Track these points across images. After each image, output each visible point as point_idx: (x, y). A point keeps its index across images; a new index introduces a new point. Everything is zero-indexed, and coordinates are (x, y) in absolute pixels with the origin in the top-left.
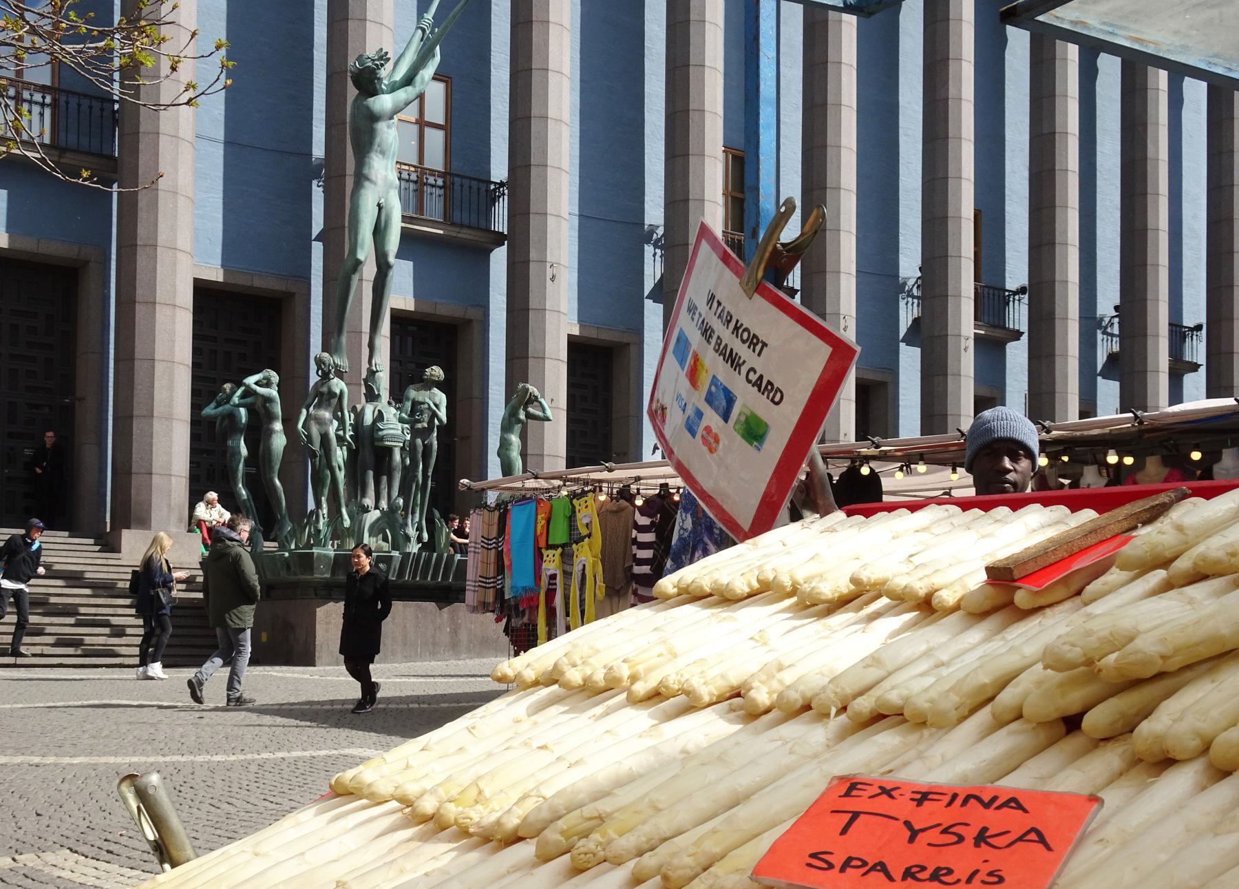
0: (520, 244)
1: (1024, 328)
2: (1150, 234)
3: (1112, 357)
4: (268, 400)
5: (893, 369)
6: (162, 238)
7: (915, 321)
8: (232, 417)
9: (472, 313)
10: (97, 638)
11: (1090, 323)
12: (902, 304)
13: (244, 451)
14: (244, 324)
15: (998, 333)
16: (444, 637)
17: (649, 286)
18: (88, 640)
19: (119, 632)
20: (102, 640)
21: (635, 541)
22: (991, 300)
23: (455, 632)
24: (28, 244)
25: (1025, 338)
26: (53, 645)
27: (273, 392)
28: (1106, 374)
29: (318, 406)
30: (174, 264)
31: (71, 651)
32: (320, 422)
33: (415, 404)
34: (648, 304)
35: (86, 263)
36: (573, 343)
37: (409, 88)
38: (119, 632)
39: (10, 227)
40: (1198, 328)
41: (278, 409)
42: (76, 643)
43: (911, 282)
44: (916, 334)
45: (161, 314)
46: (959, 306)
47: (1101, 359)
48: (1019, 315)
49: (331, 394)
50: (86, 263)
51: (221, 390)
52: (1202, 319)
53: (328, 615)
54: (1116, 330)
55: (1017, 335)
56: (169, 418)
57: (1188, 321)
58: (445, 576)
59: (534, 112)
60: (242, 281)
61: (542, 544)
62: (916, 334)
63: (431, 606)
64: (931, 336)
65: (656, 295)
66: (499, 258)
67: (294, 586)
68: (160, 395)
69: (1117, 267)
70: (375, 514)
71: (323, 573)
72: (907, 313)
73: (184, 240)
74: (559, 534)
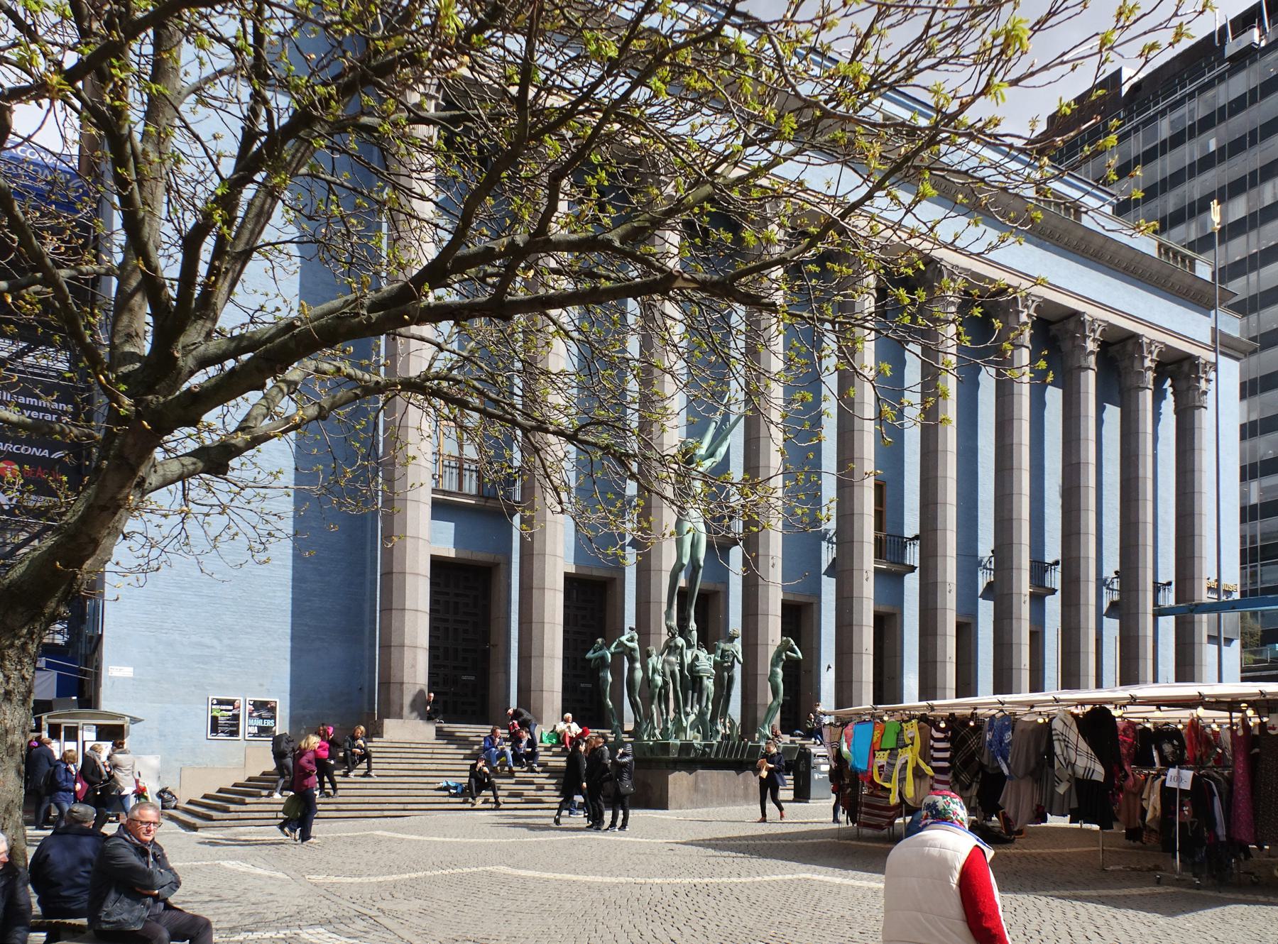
0: (752, 543)
1: (917, 564)
2: (1141, 526)
3: (1113, 604)
4: (633, 649)
5: (974, 615)
6: (548, 550)
7: (834, 560)
8: (603, 658)
9: (719, 587)
10: (530, 792)
11: (1101, 582)
12: (980, 573)
13: (610, 679)
14: (591, 599)
15: (1040, 591)
16: (740, 792)
17: (824, 567)
18: (526, 793)
19: (541, 788)
20: (533, 793)
21: (932, 747)
22: (889, 545)
23: (746, 788)
24: (466, 555)
25: (1059, 594)
26: (508, 796)
27: (635, 645)
28: (1109, 615)
29: (669, 654)
30: (555, 565)
31: (518, 800)
32: (670, 663)
33: (723, 651)
34: (824, 578)
35: (498, 564)
36: (568, 578)
37: (712, 460)
38: (541, 788)
39: (455, 546)
40: (1169, 584)
41: (638, 655)
42: (519, 795)
43: (831, 533)
44: (990, 592)
45: (409, 580)
46: (1020, 575)
47: (1106, 605)
48: (1055, 579)
49: (676, 647)
50: (498, 564)
51: (594, 642)
52: (1172, 578)
53: (675, 779)
54: (1116, 586)
55: (1053, 591)
56: (552, 657)
57: (1162, 580)
58: (742, 755)
59: (761, 464)
60: (586, 571)
61: (877, 747)
62: (990, 592)
63: (733, 772)
64: (1000, 593)
65: (831, 571)
66: (736, 553)
67: (659, 761)
68: (547, 643)
69: (1118, 546)
70: (692, 717)
71: (674, 755)
72: (828, 554)
73: (560, 550)
74: (890, 742)
